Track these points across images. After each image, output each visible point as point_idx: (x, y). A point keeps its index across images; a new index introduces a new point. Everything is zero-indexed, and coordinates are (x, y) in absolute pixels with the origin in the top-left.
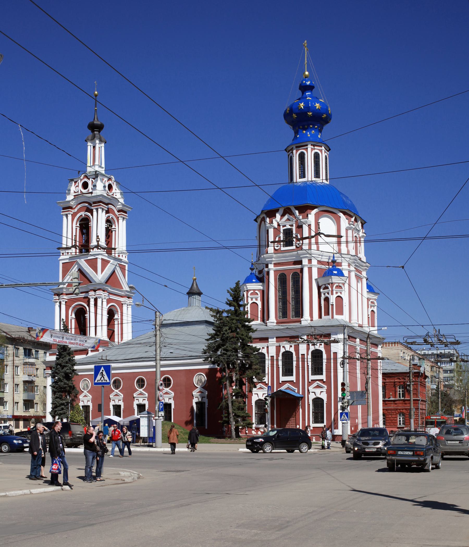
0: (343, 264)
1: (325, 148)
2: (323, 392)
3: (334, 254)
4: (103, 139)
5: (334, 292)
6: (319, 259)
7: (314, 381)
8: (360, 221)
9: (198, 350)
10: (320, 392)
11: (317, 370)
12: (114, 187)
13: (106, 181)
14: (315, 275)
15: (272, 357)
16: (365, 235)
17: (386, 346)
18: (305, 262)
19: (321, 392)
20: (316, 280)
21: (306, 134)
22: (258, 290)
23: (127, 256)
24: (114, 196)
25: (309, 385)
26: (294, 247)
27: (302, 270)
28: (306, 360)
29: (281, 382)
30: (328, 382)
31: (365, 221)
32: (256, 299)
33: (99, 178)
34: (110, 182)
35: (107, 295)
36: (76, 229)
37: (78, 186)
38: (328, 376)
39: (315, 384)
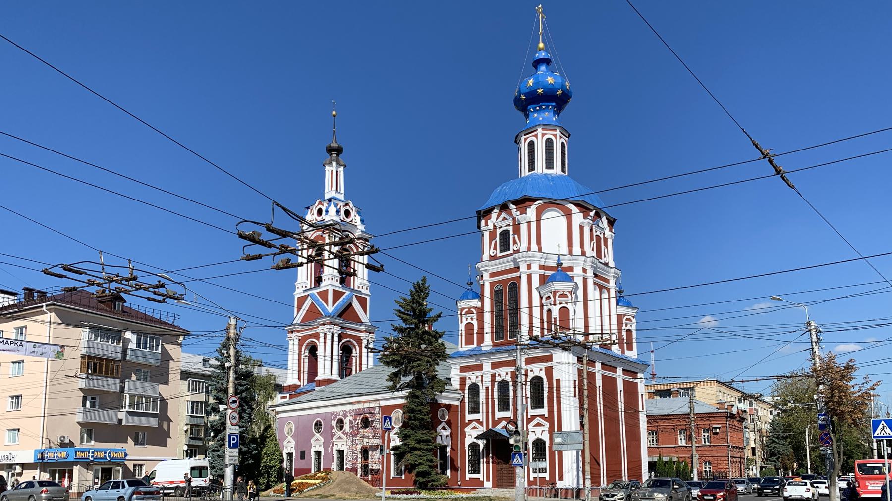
0: (575, 269)
1: (560, 132)
2: (544, 431)
4: (342, 163)
5: (464, 319)
6: (542, 264)
7: (534, 417)
8: (605, 217)
10: (541, 432)
11: (537, 402)
12: (353, 213)
13: (342, 207)
14: (536, 282)
15: (487, 388)
16: (614, 235)
17: (700, 385)
18: (523, 268)
19: (542, 431)
20: (537, 288)
21: (538, 117)
22: (474, 308)
23: (368, 288)
24: (353, 223)
25: (528, 423)
26: (511, 252)
29: (496, 419)
30: (550, 419)
31: (615, 219)
32: (472, 319)
33: (332, 202)
34: (348, 208)
35: (339, 329)
37: (313, 214)
38: (551, 411)
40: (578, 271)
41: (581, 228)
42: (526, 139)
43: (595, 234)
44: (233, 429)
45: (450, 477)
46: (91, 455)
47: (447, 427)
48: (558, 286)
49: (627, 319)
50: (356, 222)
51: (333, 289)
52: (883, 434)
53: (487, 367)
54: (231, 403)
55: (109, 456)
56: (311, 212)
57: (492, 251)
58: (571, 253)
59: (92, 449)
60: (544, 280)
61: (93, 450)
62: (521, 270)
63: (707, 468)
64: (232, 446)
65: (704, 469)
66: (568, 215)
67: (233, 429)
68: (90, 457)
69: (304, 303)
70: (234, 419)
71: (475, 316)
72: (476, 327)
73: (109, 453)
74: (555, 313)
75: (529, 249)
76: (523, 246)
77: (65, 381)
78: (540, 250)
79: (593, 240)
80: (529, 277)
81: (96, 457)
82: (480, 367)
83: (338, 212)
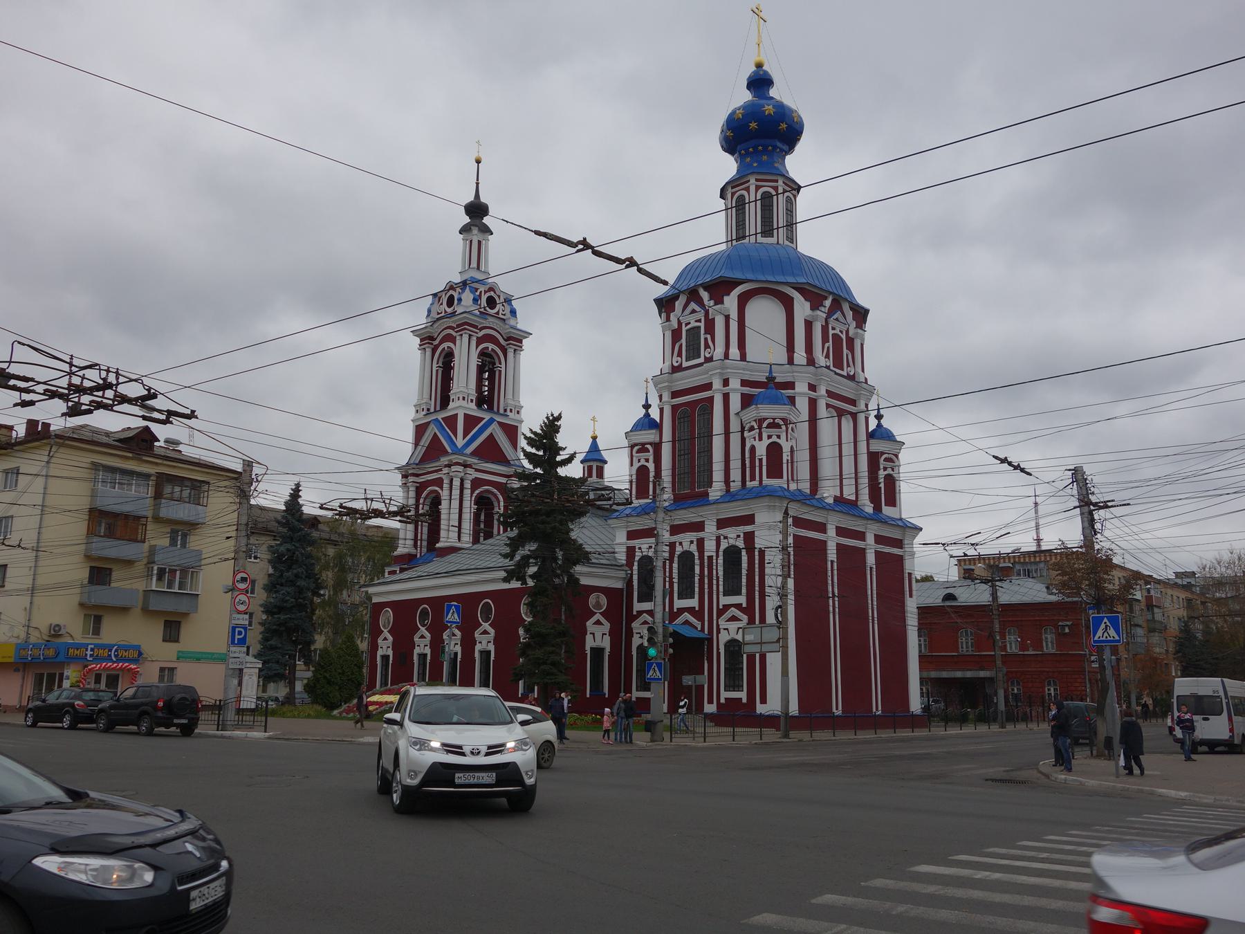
1: (784, 182)
3: (771, 365)
5: (765, 436)
7: (727, 607)
9: (12, 557)
18: (717, 384)
22: (651, 444)
24: (501, 316)
26: (701, 360)
27: (711, 399)
28: (714, 567)
29: (675, 610)
32: (647, 460)
36: (437, 370)
39: (728, 614)
40: (801, 387)
41: (809, 325)
42: (733, 194)
43: (831, 332)
44: (239, 619)
45: (607, 696)
46: (89, 653)
47: (603, 620)
48: (768, 411)
49: (886, 460)
50: (504, 315)
51: (465, 414)
52: (1106, 637)
53: (711, 527)
54: (237, 581)
55: (115, 655)
56: (439, 301)
57: (675, 358)
58: (791, 361)
59: (91, 644)
60: (747, 401)
61: (92, 646)
62: (714, 387)
63: (1052, 689)
64: (236, 642)
65: (1047, 692)
66: (788, 304)
67: (239, 619)
68: (88, 656)
69: (423, 435)
70: (242, 604)
71: (650, 456)
72: (652, 474)
73: (116, 651)
74: (761, 450)
75: (726, 356)
76: (719, 352)
77: (1032, 470)
78: (743, 357)
79: (828, 342)
80: (726, 397)
81: (97, 655)
82: (699, 527)
83: (475, 300)
